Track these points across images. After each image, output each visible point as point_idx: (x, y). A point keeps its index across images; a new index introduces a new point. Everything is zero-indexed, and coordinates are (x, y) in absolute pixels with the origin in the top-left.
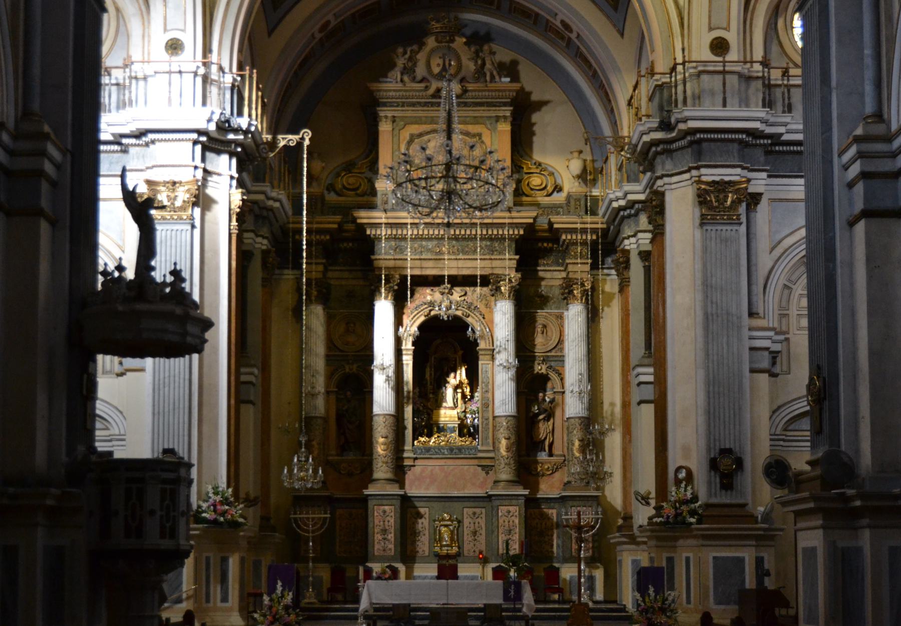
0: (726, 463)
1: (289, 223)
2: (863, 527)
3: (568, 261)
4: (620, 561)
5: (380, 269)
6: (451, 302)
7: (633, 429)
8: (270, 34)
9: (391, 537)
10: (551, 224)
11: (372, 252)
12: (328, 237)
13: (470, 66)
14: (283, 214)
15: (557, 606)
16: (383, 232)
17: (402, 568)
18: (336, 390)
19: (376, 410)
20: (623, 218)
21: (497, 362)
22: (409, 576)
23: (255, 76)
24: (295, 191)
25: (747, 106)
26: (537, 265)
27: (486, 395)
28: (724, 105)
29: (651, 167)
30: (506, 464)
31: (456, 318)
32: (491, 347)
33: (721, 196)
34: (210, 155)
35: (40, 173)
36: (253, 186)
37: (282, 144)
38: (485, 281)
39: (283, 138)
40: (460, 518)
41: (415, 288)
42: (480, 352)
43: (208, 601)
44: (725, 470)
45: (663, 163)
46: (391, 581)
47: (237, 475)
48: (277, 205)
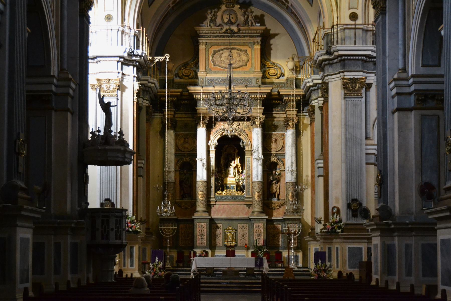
0: (354, 205)
1: (158, 92)
2: (396, 236)
3: (287, 109)
4: (310, 249)
5: (200, 113)
6: (232, 129)
7: (316, 188)
8: (149, 6)
9: (205, 237)
10: (279, 92)
11: (196, 106)
12: (176, 99)
13: (241, 19)
14: (156, 89)
15: (280, 269)
16: (201, 96)
17: (210, 252)
18: (179, 169)
19: (198, 179)
20: (312, 90)
21: (254, 157)
22: (213, 255)
23: (144, 31)
24: (160, 77)
25: (366, 44)
26: (273, 111)
27: (249, 172)
28: (355, 44)
29: (323, 70)
30: (258, 204)
31: (235, 136)
32: (251, 150)
33: (354, 85)
34: (125, 67)
35: (68, 94)
36: (142, 77)
37: (156, 61)
38: (248, 119)
39: (157, 58)
40: (236, 229)
41: (216, 122)
42: (246, 152)
43: (124, 266)
44: (354, 208)
45: (328, 69)
46: (205, 257)
47: (137, 210)
48: (153, 85)
